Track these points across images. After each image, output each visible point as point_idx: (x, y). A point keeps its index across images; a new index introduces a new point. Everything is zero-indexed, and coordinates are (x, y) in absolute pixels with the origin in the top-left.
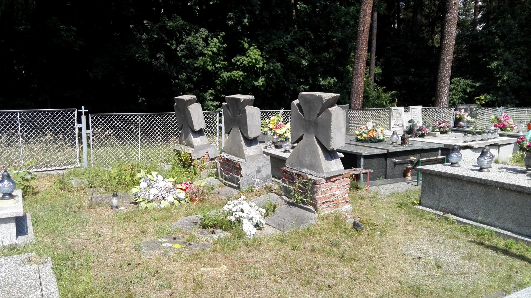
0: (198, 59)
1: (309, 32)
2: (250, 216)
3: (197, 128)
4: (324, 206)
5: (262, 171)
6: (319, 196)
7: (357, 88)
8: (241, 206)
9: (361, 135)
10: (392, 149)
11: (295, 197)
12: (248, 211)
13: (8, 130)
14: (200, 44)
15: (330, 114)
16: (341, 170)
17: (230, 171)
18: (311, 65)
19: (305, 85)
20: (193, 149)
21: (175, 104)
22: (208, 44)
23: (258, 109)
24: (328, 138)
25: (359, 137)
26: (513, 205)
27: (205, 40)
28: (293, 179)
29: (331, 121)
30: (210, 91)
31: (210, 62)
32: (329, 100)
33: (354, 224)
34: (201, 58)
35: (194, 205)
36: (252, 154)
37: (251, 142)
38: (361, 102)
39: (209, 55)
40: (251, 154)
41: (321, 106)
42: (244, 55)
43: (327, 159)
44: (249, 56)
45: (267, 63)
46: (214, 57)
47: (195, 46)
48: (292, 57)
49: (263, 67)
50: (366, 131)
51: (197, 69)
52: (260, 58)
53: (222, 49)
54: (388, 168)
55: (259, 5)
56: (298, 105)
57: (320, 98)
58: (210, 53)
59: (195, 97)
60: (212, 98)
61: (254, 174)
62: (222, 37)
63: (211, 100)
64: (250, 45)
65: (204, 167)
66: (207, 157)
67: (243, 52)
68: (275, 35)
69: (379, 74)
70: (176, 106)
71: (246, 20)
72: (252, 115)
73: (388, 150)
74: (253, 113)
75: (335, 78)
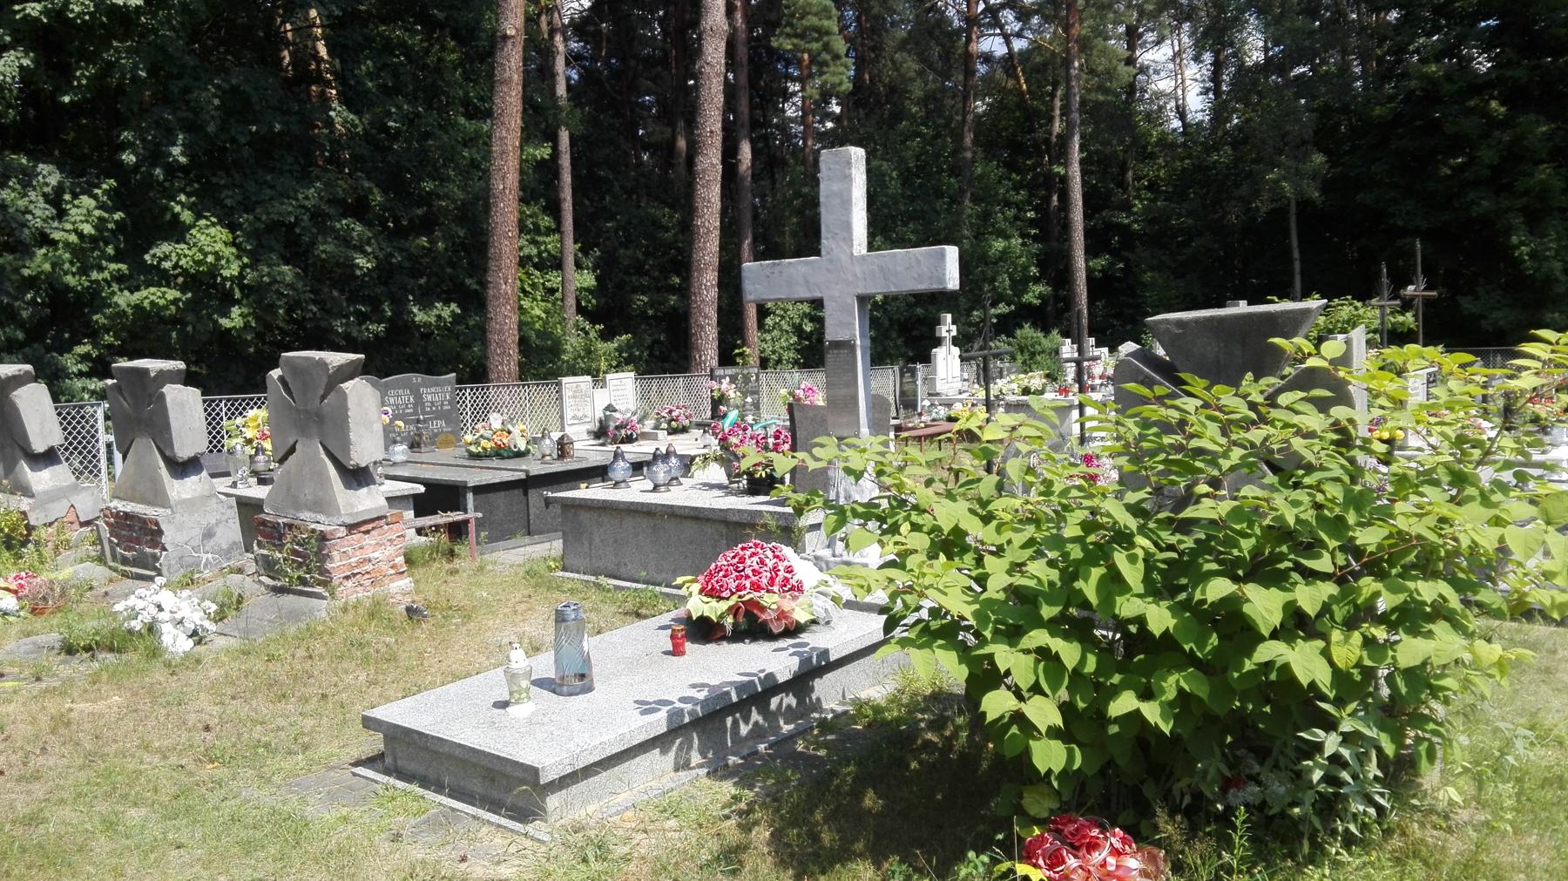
0: (32, 255)
1: (366, 184)
2: (178, 616)
3: (39, 446)
4: (349, 584)
5: (218, 534)
6: (336, 564)
7: (501, 332)
8: (156, 599)
9: (477, 443)
10: (537, 469)
11: (286, 574)
12: (169, 608)
14: (38, 213)
15: (344, 396)
16: (381, 508)
17: (134, 542)
18: (385, 271)
19: (372, 323)
20: (31, 501)
22: (61, 214)
23: (198, 392)
24: (346, 444)
25: (473, 448)
26: (691, 543)
27: (55, 200)
28: (281, 537)
29: (347, 409)
30: (80, 350)
31: (72, 263)
32: (341, 367)
33: (409, 609)
34: (43, 251)
35: (39, 623)
37: (183, 468)
38: (514, 367)
39: (67, 245)
41: (325, 380)
42: (181, 239)
43: (348, 486)
44: (195, 245)
45: (252, 266)
46: (85, 253)
47: (20, 217)
48: (326, 248)
49: (241, 276)
50: (488, 434)
51: (31, 283)
52: (229, 251)
53: (111, 226)
54: (532, 511)
55: (217, 108)
56: (281, 379)
57: (323, 364)
58: (73, 238)
59: (29, 367)
60: (84, 368)
62: (105, 192)
63: (81, 374)
64: (199, 216)
65: (68, 545)
66: (71, 517)
67: (177, 232)
68: (272, 187)
69: (586, 290)
71: (176, 151)
72: (182, 405)
73: (527, 472)
74: (185, 406)
75: (453, 306)
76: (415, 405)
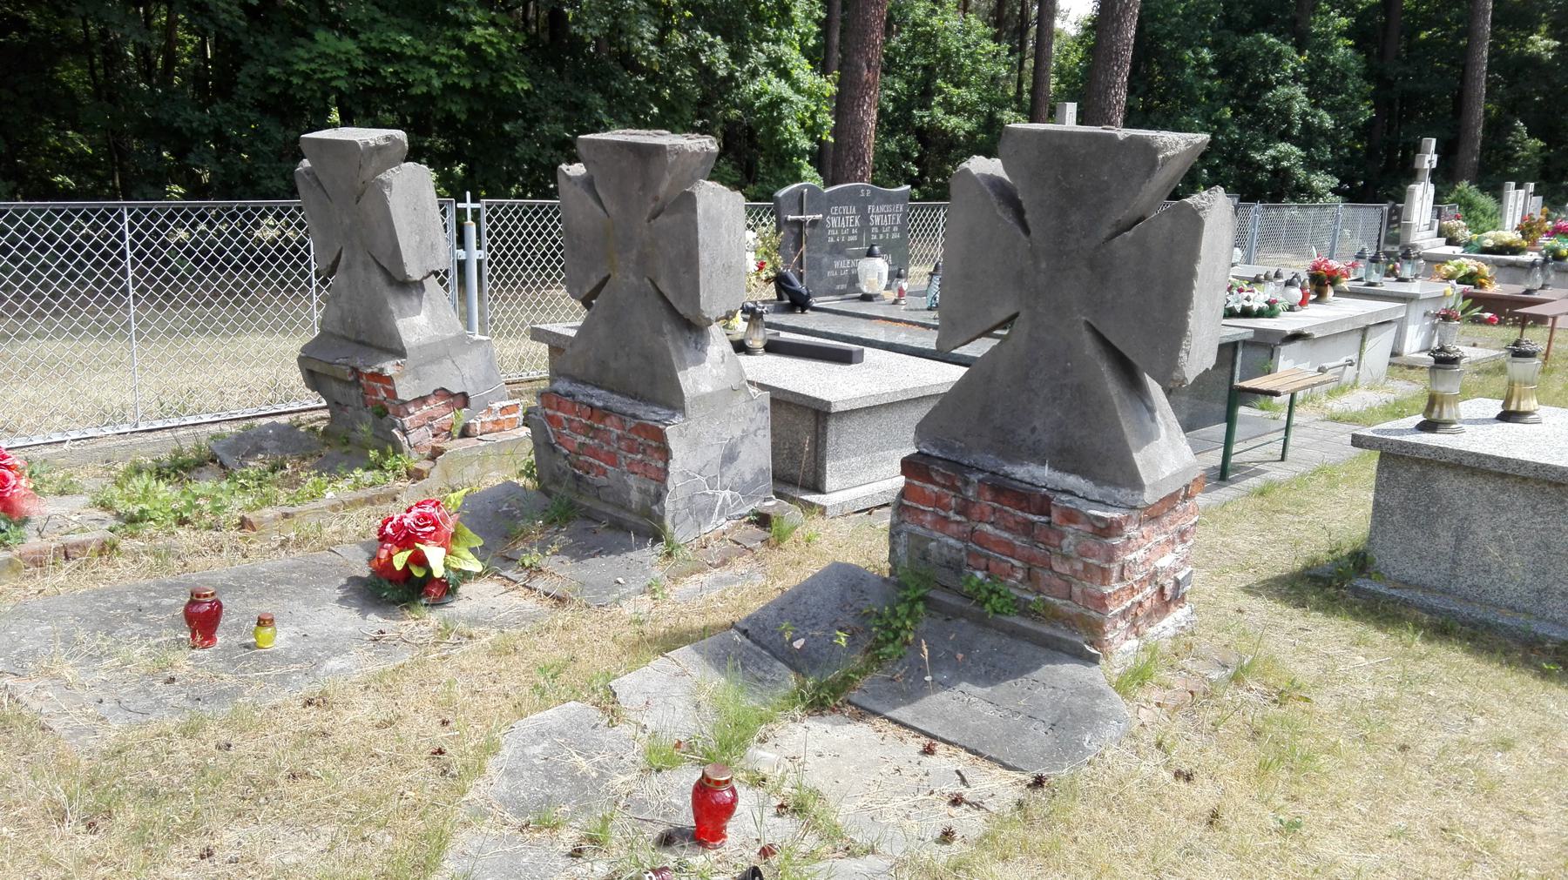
5: (742, 456)
13: (197, 243)
21: (306, 163)
36: (709, 389)
40: (706, 388)
61: (713, 470)
70: (308, 171)
76: (860, 230)
